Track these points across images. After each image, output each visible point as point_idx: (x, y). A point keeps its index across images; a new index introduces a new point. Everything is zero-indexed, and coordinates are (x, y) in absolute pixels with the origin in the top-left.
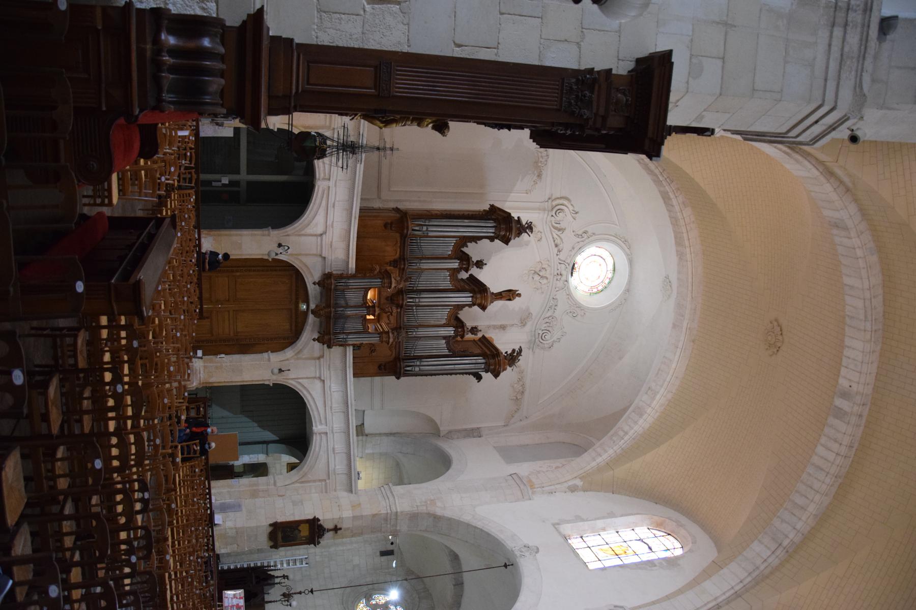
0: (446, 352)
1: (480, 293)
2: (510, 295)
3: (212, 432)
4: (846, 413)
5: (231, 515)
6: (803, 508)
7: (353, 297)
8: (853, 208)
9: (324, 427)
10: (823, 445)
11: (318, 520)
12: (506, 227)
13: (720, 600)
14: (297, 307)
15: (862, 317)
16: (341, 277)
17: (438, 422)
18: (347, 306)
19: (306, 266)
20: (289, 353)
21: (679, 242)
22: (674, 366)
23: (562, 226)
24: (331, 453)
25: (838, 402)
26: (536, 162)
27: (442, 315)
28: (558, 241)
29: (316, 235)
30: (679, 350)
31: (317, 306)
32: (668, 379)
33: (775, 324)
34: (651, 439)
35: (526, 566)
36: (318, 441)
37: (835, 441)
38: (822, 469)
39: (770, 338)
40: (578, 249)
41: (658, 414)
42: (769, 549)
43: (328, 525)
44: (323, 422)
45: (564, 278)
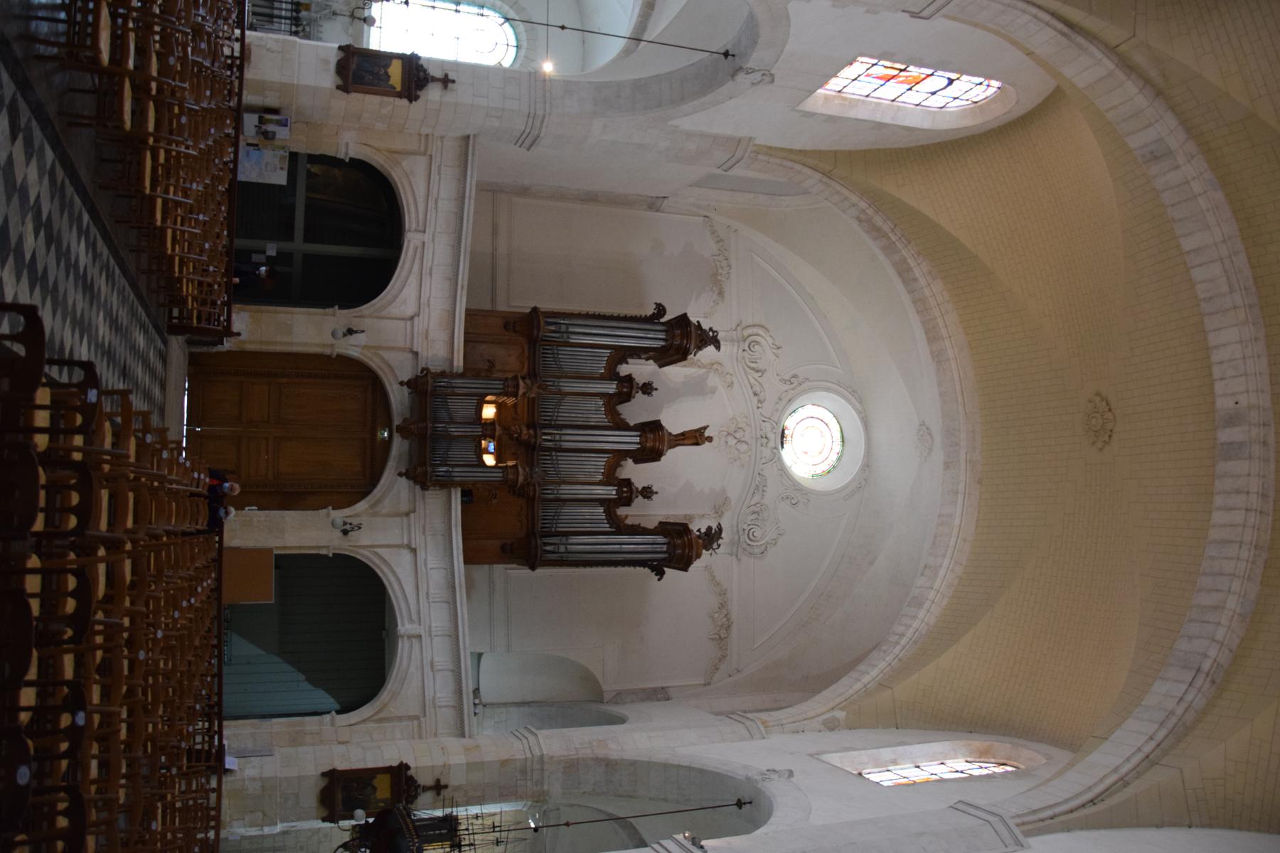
0: (606, 527)
1: (654, 440)
2: (696, 437)
3: (232, 489)
4: (1241, 444)
5: (255, 761)
6: (1219, 608)
7: (460, 408)
8: (1171, 121)
9: (415, 626)
10: (1219, 509)
11: (407, 767)
12: (682, 339)
13: (1124, 770)
14: (374, 435)
15: (1225, 289)
16: (442, 374)
17: (600, 679)
18: (452, 421)
19: (389, 366)
20: (361, 506)
21: (932, 336)
22: (957, 522)
23: (760, 366)
24: (427, 669)
25: (1225, 435)
26: (715, 275)
27: (597, 465)
28: (758, 389)
29: (404, 319)
30: (960, 498)
31: (405, 420)
32: (952, 543)
33: (1098, 399)
34: (949, 630)
35: (776, 789)
36: (406, 650)
37: (1238, 492)
38: (1231, 542)
39: (1094, 421)
40: (786, 403)
41: (946, 600)
42: (1182, 682)
43: (425, 779)
44: (415, 617)
45: (771, 444)
